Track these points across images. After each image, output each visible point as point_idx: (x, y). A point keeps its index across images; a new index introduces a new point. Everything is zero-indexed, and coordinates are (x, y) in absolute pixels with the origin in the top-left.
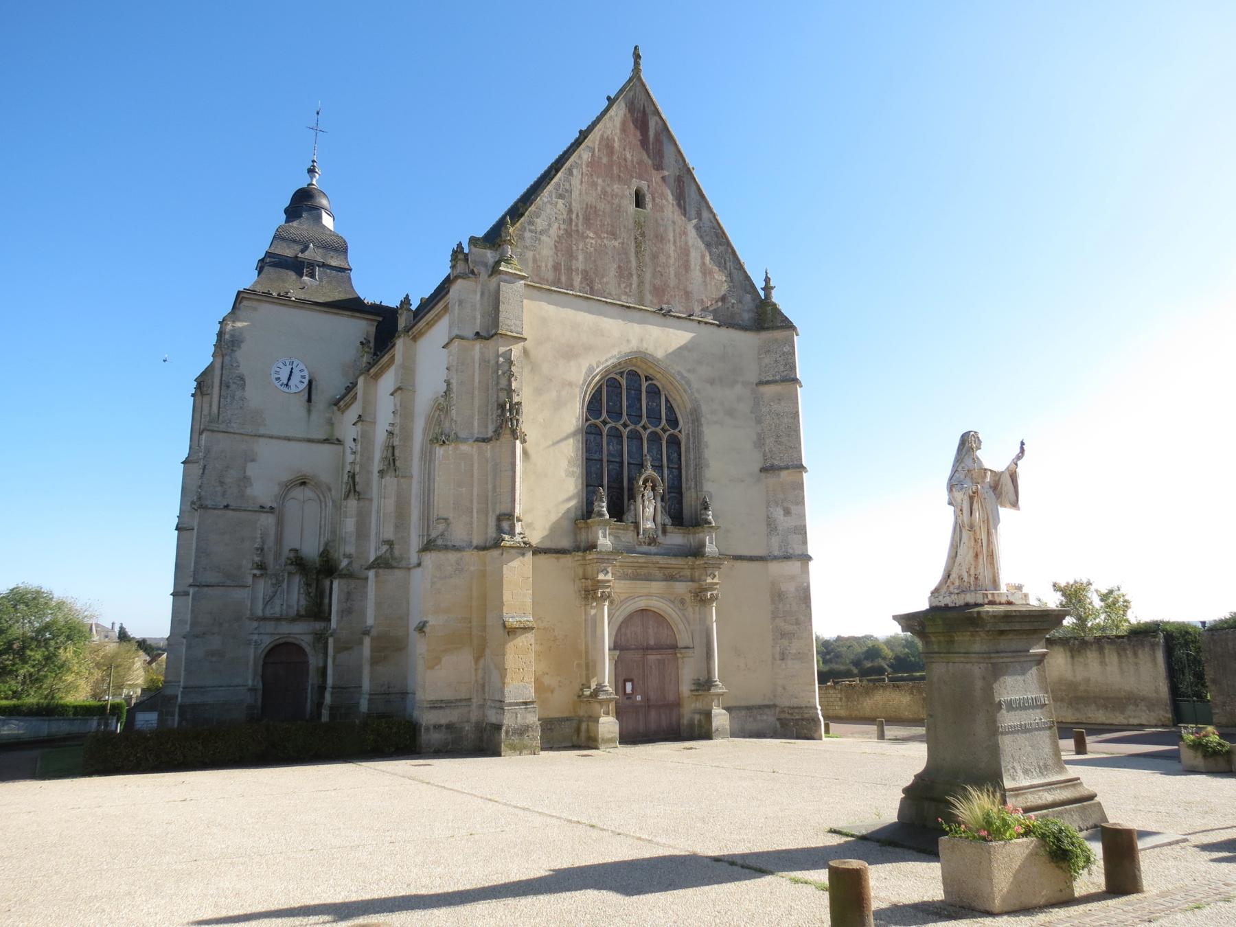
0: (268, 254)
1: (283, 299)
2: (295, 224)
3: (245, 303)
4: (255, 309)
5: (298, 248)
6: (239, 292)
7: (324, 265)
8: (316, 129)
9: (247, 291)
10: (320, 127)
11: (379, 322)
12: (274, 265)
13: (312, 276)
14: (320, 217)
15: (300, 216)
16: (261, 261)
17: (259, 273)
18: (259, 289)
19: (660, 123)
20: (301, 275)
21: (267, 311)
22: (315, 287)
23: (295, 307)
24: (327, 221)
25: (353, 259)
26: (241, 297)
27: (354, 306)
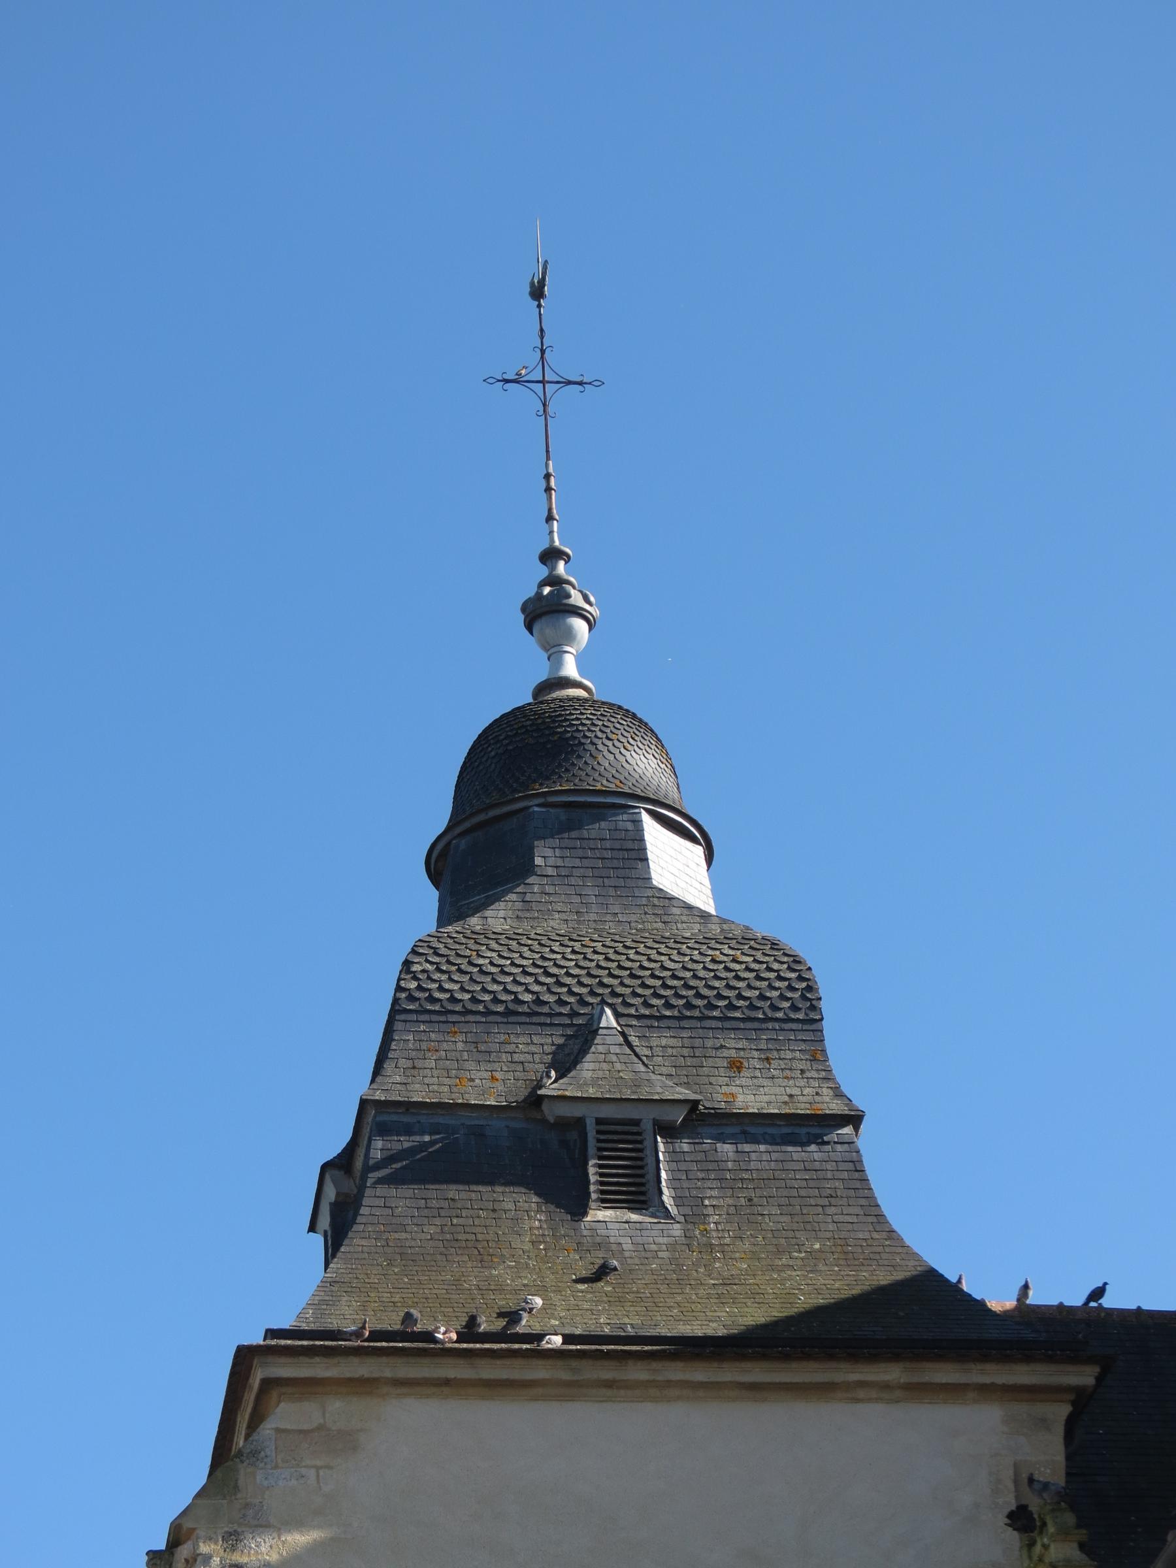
0: (373, 1116)
1: (499, 1355)
2: (498, 917)
3: (286, 1414)
4: (344, 1443)
5: (533, 1047)
6: (244, 1357)
7: (698, 1120)
8: (541, 381)
9: (283, 1343)
10: (561, 363)
11: (1081, 1400)
12: (416, 1170)
13: (637, 1193)
14: (637, 853)
15: (526, 869)
16: (340, 1166)
17: (333, 1248)
18: (345, 1317)
19: (406, 1038)
20: (578, 1209)
21: (411, 1435)
22: (673, 1257)
23: (569, 1390)
24: (675, 866)
25: (860, 1055)
26: (255, 1382)
27: (915, 1327)
